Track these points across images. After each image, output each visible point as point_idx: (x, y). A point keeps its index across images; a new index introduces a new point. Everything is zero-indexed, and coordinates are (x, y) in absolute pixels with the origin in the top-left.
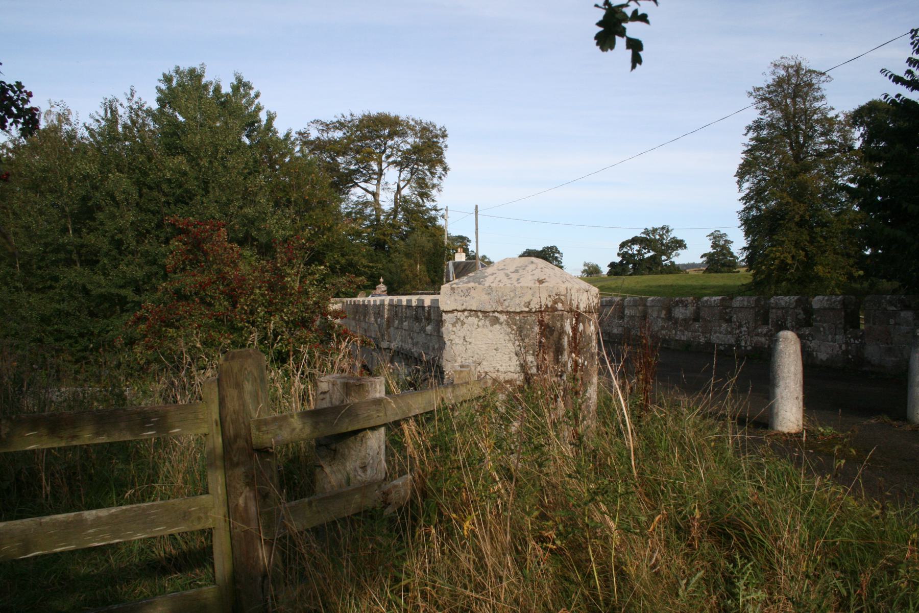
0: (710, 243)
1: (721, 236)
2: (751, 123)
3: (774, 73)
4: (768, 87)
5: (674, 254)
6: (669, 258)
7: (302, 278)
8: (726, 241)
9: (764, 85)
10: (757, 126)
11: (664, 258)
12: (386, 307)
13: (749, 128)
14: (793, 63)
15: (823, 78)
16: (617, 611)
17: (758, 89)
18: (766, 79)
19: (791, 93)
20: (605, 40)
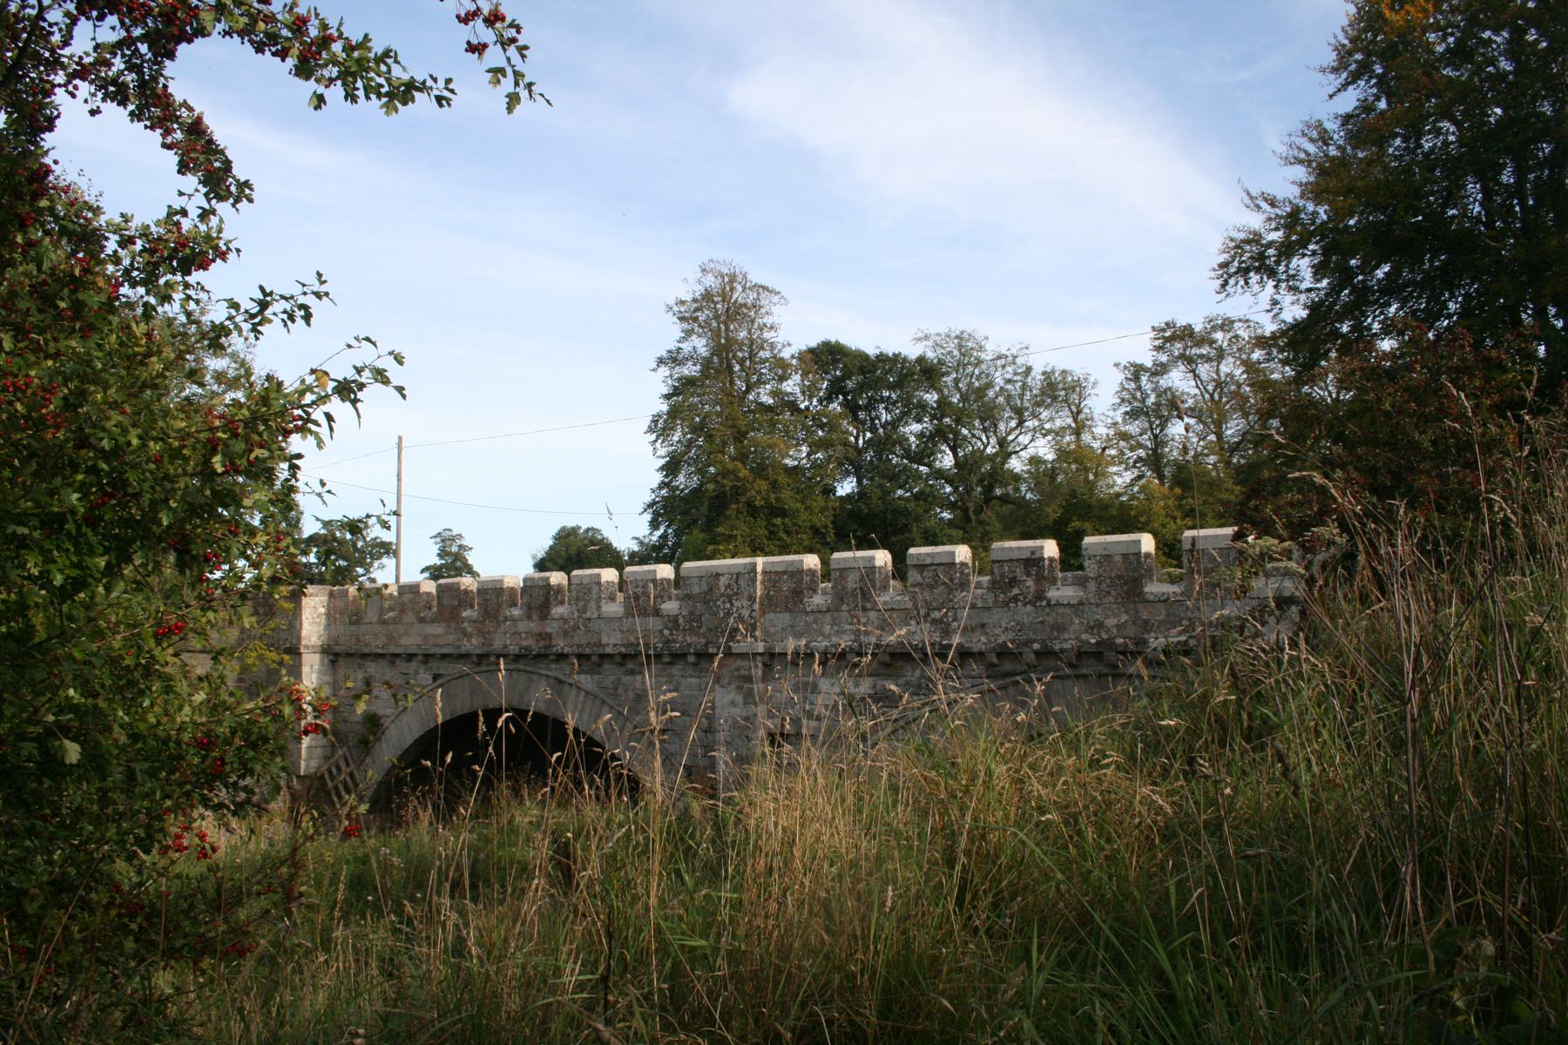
0: (435, 549)
1: (452, 539)
2: (664, 354)
3: (700, 282)
4: (695, 300)
5: (376, 564)
6: (368, 571)
7: (626, 966)
8: (460, 546)
9: (688, 298)
10: (673, 359)
11: (360, 570)
12: (759, 577)
13: (661, 361)
14: (726, 271)
15: (775, 299)
16: (1217, 1026)
17: (683, 302)
18: (688, 290)
19: (723, 315)
20: (441, 105)
